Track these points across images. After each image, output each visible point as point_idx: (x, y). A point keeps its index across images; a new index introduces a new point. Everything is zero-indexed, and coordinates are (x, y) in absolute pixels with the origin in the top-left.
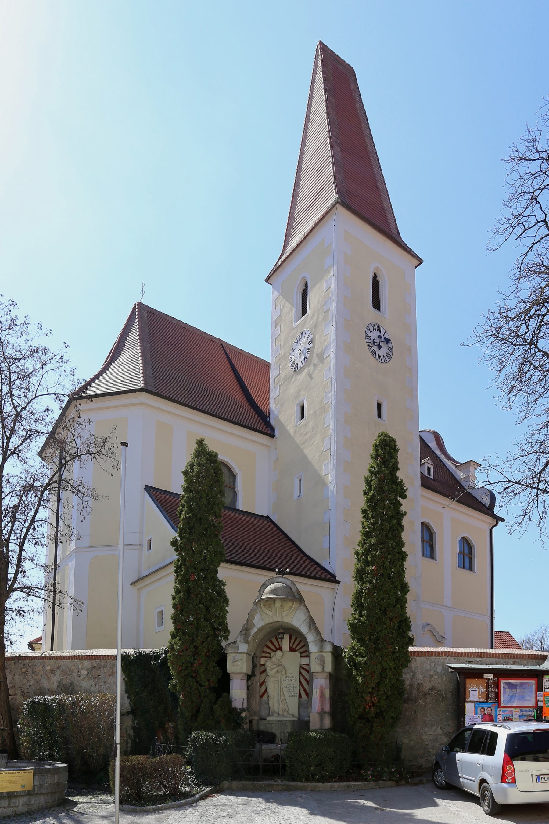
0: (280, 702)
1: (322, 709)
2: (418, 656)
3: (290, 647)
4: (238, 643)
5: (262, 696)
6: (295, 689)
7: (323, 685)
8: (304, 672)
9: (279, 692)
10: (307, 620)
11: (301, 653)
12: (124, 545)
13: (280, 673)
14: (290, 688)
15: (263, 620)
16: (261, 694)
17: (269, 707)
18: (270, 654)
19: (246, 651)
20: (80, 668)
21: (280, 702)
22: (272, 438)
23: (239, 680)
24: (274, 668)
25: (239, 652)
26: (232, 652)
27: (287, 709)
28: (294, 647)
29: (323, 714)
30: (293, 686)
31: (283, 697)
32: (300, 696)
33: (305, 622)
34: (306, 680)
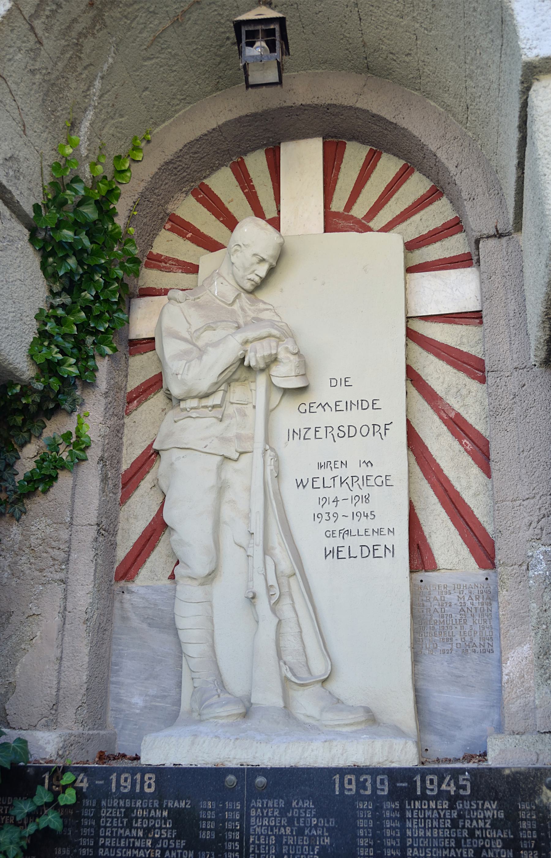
0: (263, 604)
2: (275, 155)
6: (375, 492)
9: (258, 528)
12: (295, 574)
14: (342, 492)
17: (180, 654)
20: (76, 42)
21: (263, 604)
24: (215, 345)
30: (364, 471)
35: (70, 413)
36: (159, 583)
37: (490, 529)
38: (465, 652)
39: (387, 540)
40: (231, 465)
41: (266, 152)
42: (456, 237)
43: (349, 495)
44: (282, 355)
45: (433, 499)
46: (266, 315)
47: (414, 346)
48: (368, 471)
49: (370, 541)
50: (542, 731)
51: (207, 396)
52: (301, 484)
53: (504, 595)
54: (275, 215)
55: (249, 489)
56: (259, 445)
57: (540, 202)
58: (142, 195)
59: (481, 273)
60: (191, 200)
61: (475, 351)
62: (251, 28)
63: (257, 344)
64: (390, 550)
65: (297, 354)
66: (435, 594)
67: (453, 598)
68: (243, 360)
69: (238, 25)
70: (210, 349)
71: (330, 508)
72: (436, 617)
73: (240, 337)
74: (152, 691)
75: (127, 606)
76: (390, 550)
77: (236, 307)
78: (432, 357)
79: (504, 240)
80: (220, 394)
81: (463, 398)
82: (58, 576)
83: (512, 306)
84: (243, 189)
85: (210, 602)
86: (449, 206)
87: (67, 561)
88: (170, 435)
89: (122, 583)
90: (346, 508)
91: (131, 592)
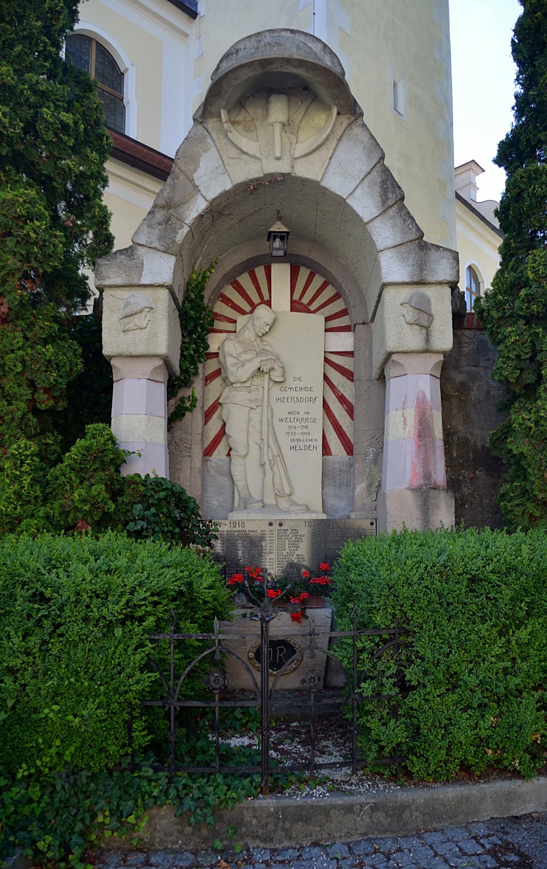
1: (427, 476)
3: (292, 301)
4: (141, 251)
5: (208, 452)
6: (310, 424)
7: (424, 397)
8: (336, 377)
9: (265, 437)
10: (374, 173)
11: (327, 319)
13: (267, 376)
14: (297, 424)
15: (226, 172)
16: (207, 444)
18: (235, 322)
19: (166, 277)
21: (268, 467)
22: (191, 19)
23: (144, 382)
24: (249, 361)
25: (144, 281)
26: (119, 281)
27: (287, 490)
28: (305, 301)
29: (432, 493)
30: (306, 416)
31: (276, 452)
32: (326, 450)
33: (366, 182)
34: (342, 399)
35: (189, 387)
36: (222, 458)
37: (352, 440)
38: (341, 486)
39: (314, 443)
40: (253, 410)
41: (265, 267)
42: (345, 317)
43: (300, 425)
44: (276, 367)
45: (331, 428)
46: (267, 348)
47: (327, 365)
48: (308, 416)
49: (308, 444)
50: (240, 661)
51: (245, 382)
52: (281, 420)
53: (357, 465)
54: (268, 298)
55: (261, 422)
56: (265, 404)
57: (382, 318)
58: (215, 289)
59: (355, 336)
60: (230, 287)
61: (351, 368)
62: (275, 234)
63: (266, 363)
64: (315, 447)
65: (283, 368)
66: (330, 464)
67: (337, 466)
68: (259, 369)
69: (270, 233)
70: (247, 363)
71: (293, 430)
72: (330, 473)
73: (259, 359)
74: (221, 499)
75: (209, 466)
76: (315, 447)
77: (255, 343)
78: (333, 369)
79: (366, 326)
80: (250, 382)
81: (345, 387)
82: (188, 454)
83: (367, 355)
84: (254, 284)
85: (245, 465)
86: (343, 303)
87: (190, 448)
88: (228, 397)
89: (207, 457)
90: (299, 430)
91: (210, 461)
